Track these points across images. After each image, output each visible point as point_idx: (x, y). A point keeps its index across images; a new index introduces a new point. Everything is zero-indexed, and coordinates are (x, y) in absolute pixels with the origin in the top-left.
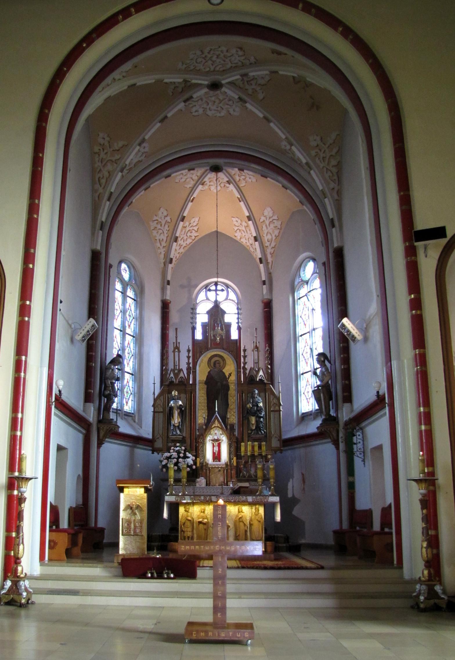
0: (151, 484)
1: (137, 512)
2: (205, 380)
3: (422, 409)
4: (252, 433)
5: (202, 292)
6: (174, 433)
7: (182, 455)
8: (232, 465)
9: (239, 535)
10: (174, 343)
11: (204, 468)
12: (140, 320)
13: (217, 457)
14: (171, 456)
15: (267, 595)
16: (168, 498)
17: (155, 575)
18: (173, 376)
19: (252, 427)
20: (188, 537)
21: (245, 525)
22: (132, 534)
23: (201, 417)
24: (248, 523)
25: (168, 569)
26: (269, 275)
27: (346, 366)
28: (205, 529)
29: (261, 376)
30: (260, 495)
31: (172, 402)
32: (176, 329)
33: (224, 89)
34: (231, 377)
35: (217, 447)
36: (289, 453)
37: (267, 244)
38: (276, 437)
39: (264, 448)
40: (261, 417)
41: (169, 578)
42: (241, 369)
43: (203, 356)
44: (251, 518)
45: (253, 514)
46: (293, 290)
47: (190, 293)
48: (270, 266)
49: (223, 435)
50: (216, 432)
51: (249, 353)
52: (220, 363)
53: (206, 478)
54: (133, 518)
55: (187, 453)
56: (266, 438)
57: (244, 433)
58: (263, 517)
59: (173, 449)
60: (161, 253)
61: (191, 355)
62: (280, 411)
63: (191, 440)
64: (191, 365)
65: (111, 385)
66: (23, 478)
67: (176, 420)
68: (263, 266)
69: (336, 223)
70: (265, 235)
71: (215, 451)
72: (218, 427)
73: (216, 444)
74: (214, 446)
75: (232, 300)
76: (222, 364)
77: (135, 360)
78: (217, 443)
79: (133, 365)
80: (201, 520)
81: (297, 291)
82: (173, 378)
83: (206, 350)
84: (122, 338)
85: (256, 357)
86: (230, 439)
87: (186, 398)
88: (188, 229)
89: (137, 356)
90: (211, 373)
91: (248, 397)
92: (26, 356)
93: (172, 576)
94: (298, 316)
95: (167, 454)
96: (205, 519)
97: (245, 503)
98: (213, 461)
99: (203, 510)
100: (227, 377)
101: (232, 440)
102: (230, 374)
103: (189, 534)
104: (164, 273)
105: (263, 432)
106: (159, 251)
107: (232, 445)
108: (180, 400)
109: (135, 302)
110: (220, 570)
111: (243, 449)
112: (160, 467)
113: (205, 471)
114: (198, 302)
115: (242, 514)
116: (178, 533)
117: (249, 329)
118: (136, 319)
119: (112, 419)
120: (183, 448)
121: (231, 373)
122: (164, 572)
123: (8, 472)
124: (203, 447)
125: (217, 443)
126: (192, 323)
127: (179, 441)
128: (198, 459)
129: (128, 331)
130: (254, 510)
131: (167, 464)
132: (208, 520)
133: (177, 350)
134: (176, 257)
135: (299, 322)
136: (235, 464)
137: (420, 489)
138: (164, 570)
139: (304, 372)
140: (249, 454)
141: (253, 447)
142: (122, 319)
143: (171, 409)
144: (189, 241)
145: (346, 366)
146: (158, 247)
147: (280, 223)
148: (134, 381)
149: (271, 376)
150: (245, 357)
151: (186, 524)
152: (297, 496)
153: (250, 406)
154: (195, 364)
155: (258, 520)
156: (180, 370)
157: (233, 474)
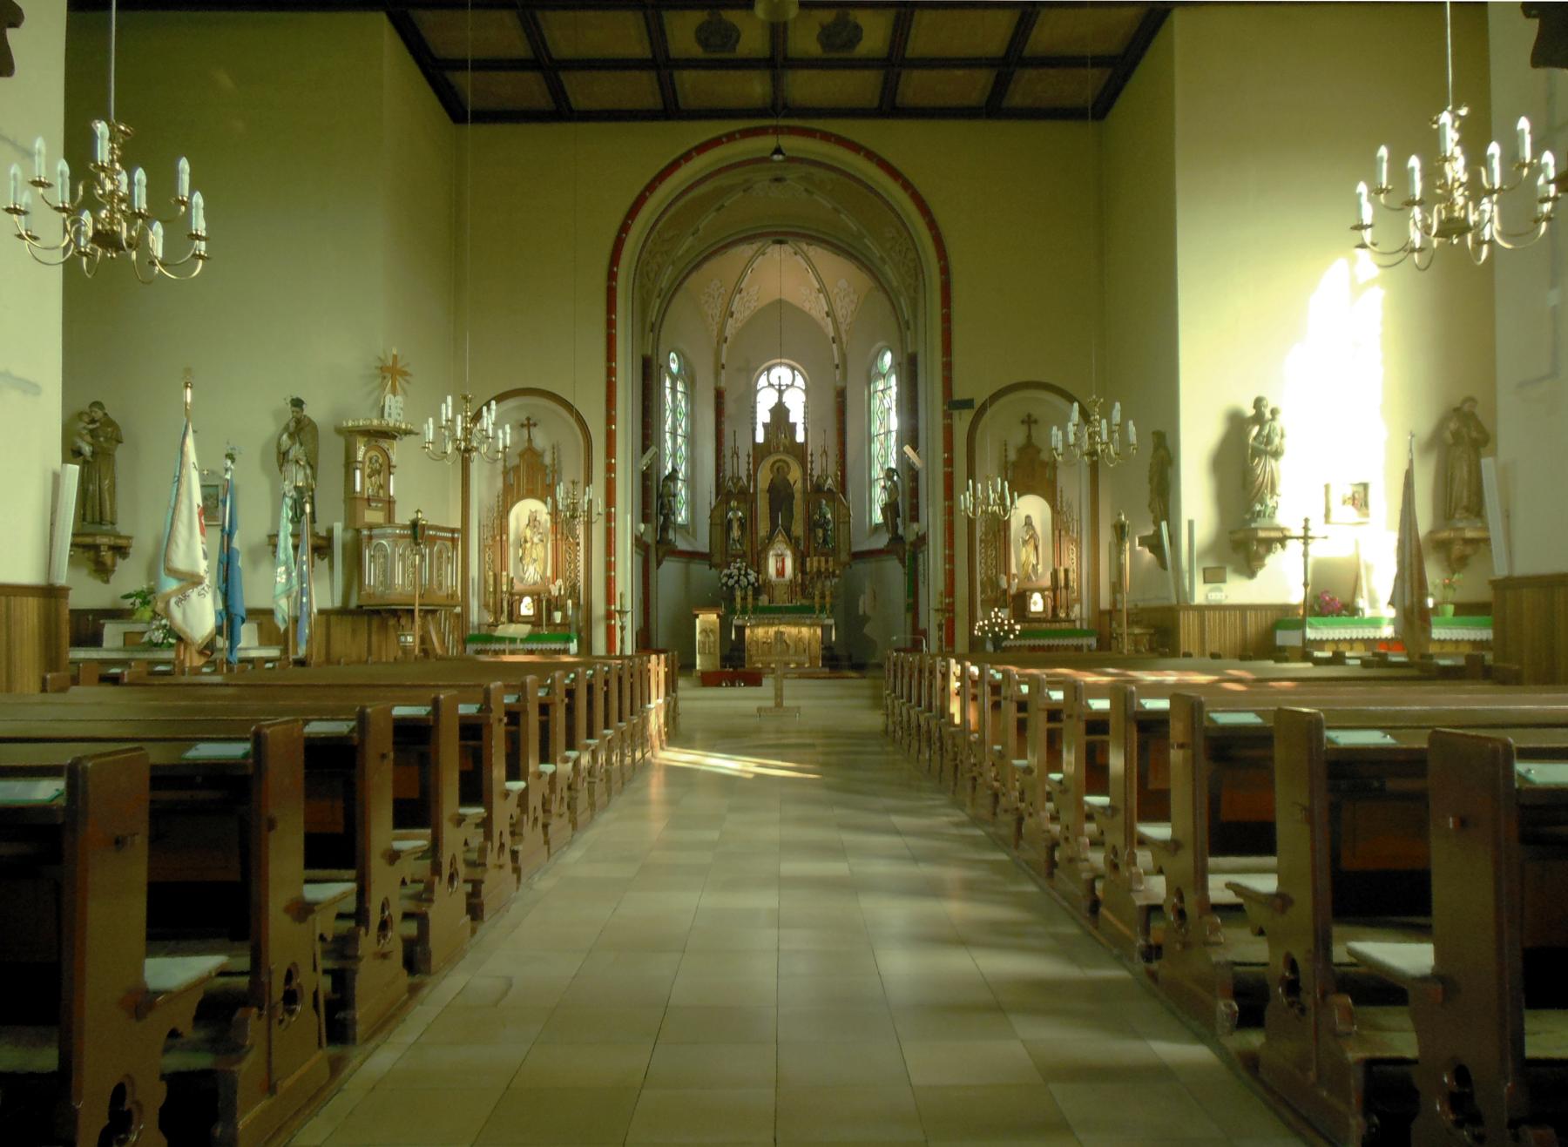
3: (947, 552)
12: (692, 417)
13: (780, 573)
23: (763, 528)
26: (844, 357)
31: (730, 514)
32: (735, 432)
33: (788, 182)
36: (860, 567)
37: (842, 320)
39: (831, 563)
41: (740, 686)
51: (817, 458)
53: (769, 596)
56: (835, 552)
67: (736, 533)
69: (912, 327)
70: (839, 309)
75: (799, 387)
76: (786, 470)
78: (781, 558)
80: (765, 640)
85: (824, 465)
86: (794, 554)
88: (745, 299)
95: (726, 571)
97: (804, 625)
104: (718, 354)
111: (808, 564)
112: (720, 585)
114: (758, 388)
119: (671, 540)
120: (744, 564)
125: (781, 558)
126: (752, 424)
127: (740, 557)
128: (760, 576)
130: (812, 631)
131: (727, 582)
136: (800, 581)
140: (815, 570)
141: (819, 561)
143: (730, 521)
144: (747, 313)
147: (856, 297)
148: (687, 488)
149: (843, 484)
150: (812, 462)
156: (739, 478)
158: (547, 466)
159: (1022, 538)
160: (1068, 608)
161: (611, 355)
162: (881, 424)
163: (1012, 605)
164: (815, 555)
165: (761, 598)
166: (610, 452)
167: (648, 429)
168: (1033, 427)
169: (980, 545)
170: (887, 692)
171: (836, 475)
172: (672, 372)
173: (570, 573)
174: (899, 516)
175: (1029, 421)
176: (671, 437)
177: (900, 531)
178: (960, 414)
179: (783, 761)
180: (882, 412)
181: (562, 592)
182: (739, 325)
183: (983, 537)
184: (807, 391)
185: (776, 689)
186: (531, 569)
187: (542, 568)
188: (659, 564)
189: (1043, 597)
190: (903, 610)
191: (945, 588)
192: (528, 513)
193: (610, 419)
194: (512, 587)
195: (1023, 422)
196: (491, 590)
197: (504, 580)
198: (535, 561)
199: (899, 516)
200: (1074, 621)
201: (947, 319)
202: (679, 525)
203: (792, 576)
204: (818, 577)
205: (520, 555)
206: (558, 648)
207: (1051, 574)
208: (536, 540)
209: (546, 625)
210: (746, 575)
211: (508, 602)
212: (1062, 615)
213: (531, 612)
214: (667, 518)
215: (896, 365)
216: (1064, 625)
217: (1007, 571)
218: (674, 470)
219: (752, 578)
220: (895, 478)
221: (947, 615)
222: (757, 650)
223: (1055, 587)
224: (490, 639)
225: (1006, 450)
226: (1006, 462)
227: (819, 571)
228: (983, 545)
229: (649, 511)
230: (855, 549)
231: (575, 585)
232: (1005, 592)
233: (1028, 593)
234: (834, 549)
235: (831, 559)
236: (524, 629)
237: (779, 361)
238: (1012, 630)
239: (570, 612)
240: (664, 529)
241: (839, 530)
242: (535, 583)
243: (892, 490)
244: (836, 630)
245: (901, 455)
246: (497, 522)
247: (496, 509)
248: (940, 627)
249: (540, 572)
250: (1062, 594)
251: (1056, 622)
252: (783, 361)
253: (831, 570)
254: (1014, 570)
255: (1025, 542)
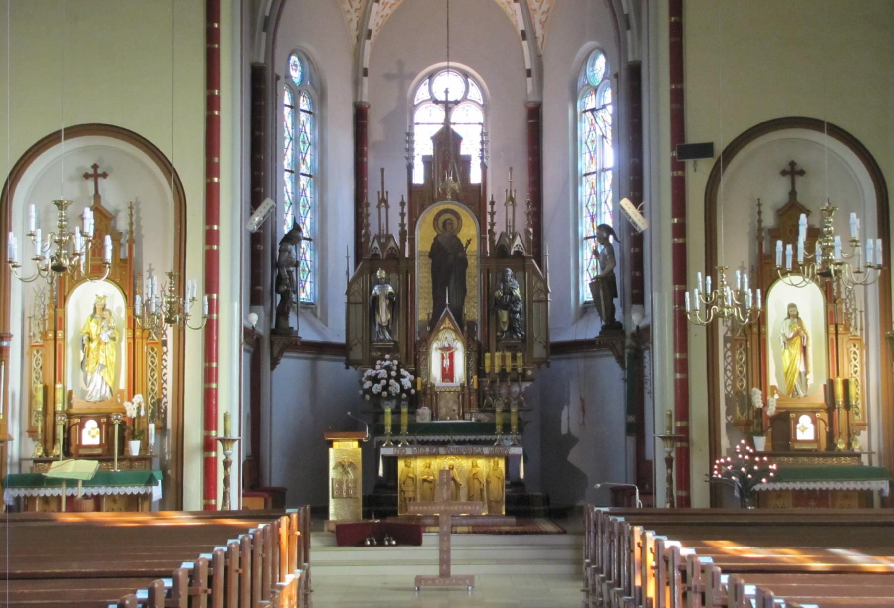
0: (367, 436)
1: (349, 469)
2: (429, 250)
4: (503, 335)
5: (423, 85)
6: (382, 337)
7: (394, 374)
8: (472, 387)
9: (473, 496)
10: (379, 193)
11: (428, 391)
12: (321, 146)
13: (448, 374)
14: (377, 375)
15: (498, 562)
16: (385, 451)
17: (375, 542)
18: (378, 247)
19: (503, 327)
20: (410, 499)
21: (480, 483)
22: (345, 497)
23: (423, 310)
24: (485, 480)
25: (389, 536)
26: (539, 59)
27: (637, 250)
28: (431, 489)
29: (517, 246)
30: (499, 445)
31: (376, 288)
32: (383, 170)
34: (470, 246)
35: (448, 360)
36: (563, 365)
38: (540, 342)
40: (516, 313)
41: (390, 545)
42: (486, 234)
43: (424, 213)
44: (489, 474)
45: (491, 468)
46: (574, 96)
47: (402, 90)
48: (539, 42)
49: (457, 341)
50: (447, 335)
51: (499, 208)
52: (453, 224)
53: (431, 408)
54: (345, 478)
55: (402, 370)
56: (525, 344)
57: (491, 336)
58: (504, 472)
59: (380, 364)
60: (351, 20)
61: (406, 210)
62: (546, 301)
63: (407, 345)
64: (406, 228)
65: (288, 277)
66: (229, 440)
68: (527, 45)
71: (444, 366)
72: (449, 328)
73: (446, 355)
74: (443, 358)
77: (315, 214)
78: (448, 353)
79: (311, 223)
80: (425, 477)
81: (581, 99)
82: (377, 249)
83: (431, 201)
84: (293, 184)
85: (510, 216)
86: (468, 347)
87: (399, 279)
89: (317, 208)
90: (439, 239)
91: (496, 277)
92: (217, 293)
93: (394, 542)
94: (581, 141)
95: (370, 372)
96: (431, 475)
97: (480, 455)
98: (443, 381)
99: (428, 465)
100: (465, 246)
101: (472, 348)
102: (469, 242)
103: (411, 495)
105: (519, 335)
106: (348, 17)
107: (471, 356)
108: (389, 284)
109: (312, 115)
110: (445, 527)
111: (487, 362)
112: (361, 392)
113: (429, 397)
114: (416, 103)
115: (477, 469)
116: (397, 493)
117: (502, 153)
118: (315, 147)
119: (292, 328)
120: (396, 362)
121: (471, 239)
122: (385, 539)
123: (203, 431)
124: (426, 359)
125: (448, 353)
126: (407, 158)
127: (388, 350)
128: (419, 379)
129: (304, 169)
130: (492, 464)
131: (371, 388)
132: (434, 477)
133: (383, 204)
134: (378, 24)
135: (583, 152)
136: (475, 386)
137: (665, 447)
138: (385, 536)
139: (588, 236)
140: (497, 370)
141: (503, 358)
142: (294, 152)
143: (376, 299)
145: (637, 250)
146: (346, 10)
148: (314, 250)
150: (493, 214)
151: (407, 482)
152: (575, 431)
153: (499, 293)
154: (412, 225)
155: (496, 476)
156: (389, 237)
157: (472, 401)
158: (121, 233)
159: (784, 335)
160: (849, 435)
161: (212, 79)
162: (591, 158)
163: (770, 430)
164: (497, 350)
165: (420, 411)
166: (211, 214)
167: (259, 152)
168: (799, 180)
169: (725, 346)
170: (587, 561)
171: (527, 232)
172: (293, 82)
173: (153, 384)
174: (616, 296)
175: (793, 171)
176: (291, 178)
177: (618, 316)
178: (695, 163)
179: (570, 259)
180: (592, 141)
181: (142, 413)
182: (388, 11)
183: (729, 334)
184: (485, 107)
185: (442, 552)
186: (97, 379)
187: (113, 377)
188: (274, 363)
189: (814, 421)
190: (622, 429)
191: (676, 406)
192: (93, 300)
193: (211, 169)
194: (70, 406)
195: (784, 173)
196: (40, 409)
197: (59, 395)
198: (103, 367)
199: (616, 296)
200: (859, 455)
201: (677, 31)
202: (302, 303)
203: (464, 380)
204: (501, 381)
205: (82, 358)
206: (135, 493)
207: (825, 386)
208: (105, 337)
209: (119, 460)
210: (399, 378)
211: (64, 426)
212: (841, 446)
213: (96, 441)
214: (285, 297)
215: (613, 76)
216: (846, 461)
217: (762, 382)
218: (296, 228)
219: (407, 383)
220: (611, 238)
221: (679, 445)
222: (415, 491)
223: (831, 406)
224: (39, 481)
225: (760, 213)
226: (760, 229)
227: (503, 372)
228: (728, 345)
229: (261, 288)
230: (555, 338)
231: (160, 401)
232: (760, 412)
233: (792, 415)
234: (524, 340)
235: (519, 354)
236: (86, 468)
237: (445, 64)
238: (765, 472)
239: (152, 441)
240: (282, 312)
241: (531, 311)
242: (102, 400)
243: (605, 257)
244: (525, 462)
245: (619, 213)
246: (49, 312)
247: (48, 294)
248: (669, 462)
249: (110, 384)
250: (841, 415)
251: (832, 456)
252: (452, 64)
253: (520, 370)
254: (772, 381)
255: (788, 341)
